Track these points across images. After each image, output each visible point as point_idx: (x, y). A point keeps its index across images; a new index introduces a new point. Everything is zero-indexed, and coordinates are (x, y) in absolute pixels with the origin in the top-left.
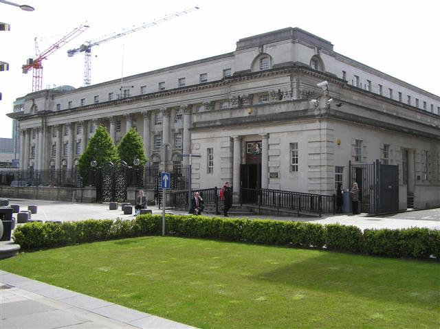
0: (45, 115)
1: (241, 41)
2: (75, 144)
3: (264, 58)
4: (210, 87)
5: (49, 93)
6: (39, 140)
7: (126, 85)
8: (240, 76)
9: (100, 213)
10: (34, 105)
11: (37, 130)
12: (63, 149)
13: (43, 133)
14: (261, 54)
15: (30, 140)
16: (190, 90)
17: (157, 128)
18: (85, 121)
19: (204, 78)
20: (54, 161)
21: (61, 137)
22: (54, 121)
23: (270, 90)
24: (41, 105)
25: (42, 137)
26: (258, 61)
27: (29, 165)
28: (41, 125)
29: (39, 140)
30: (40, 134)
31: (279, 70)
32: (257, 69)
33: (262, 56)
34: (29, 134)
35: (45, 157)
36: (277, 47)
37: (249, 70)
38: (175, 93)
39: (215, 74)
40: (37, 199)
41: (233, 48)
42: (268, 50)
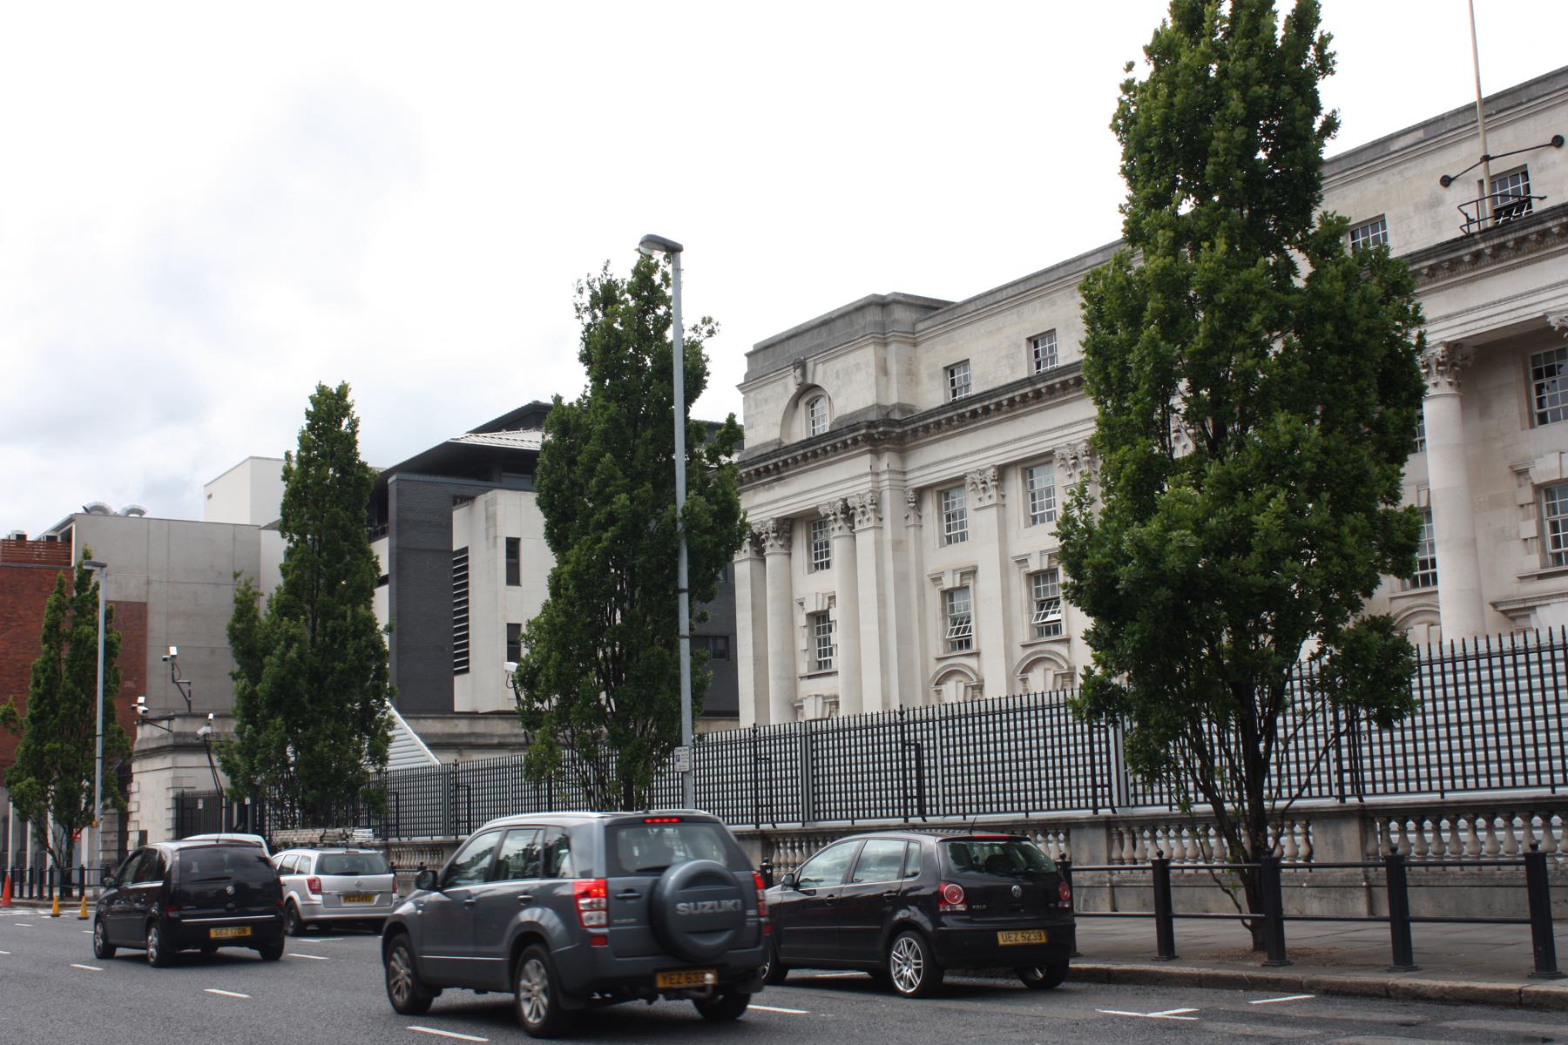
0: (890, 432)
24: (853, 386)
34: (788, 545)
38: (805, 457)
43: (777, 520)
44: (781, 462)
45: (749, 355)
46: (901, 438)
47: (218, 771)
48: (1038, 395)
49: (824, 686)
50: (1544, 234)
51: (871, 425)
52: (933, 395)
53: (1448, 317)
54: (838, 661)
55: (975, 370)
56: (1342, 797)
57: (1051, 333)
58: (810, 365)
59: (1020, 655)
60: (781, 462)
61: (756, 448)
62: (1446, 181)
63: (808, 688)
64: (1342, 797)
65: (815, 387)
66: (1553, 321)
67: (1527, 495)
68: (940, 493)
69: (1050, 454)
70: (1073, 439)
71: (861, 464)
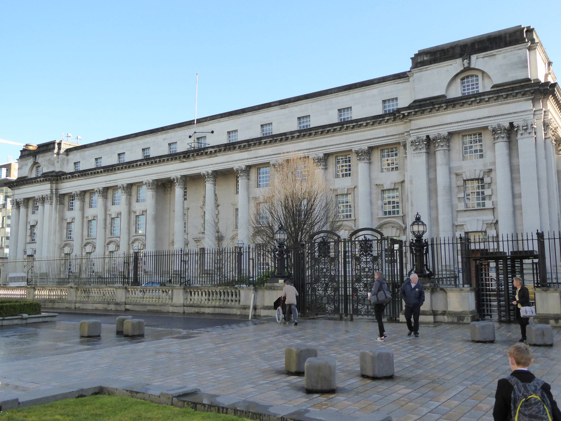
2: (109, 221)
3: (467, 77)
4: (101, 172)
6: (47, 215)
8: (433, 104)
9: (67, 345)
10: (35, 163)
11: (43, 200)
12: (108, 226)
13: (51, 204)
14: (468, 69)
16: (276, 140)
17: (90, 212)
18: (25, 199)
19: (147, 153)
20: (71, 247)
21: (82, 209)
26: (458, 81)
27: (25, 252)
28: (48, 192)
29: (47, 215)
30: (47, 206)
32: (456, 92)
33: (467, 73)
34: (27, 207)
36: (497, 56)
38: (140, 165)
39: (367, 105)
41: (406, 66)
42: (478, 61)
45: (412, 58)
47: (105, 306)
49: (33, 246)
52: (70, 168)
54: (37, 239)
55: (81, 164)
57: (236, 131)
62: (195, 132)
63: (29, 246)
65: (37, 163)
66: (235, 169)
68: (90, 193)
69: (269, 163)
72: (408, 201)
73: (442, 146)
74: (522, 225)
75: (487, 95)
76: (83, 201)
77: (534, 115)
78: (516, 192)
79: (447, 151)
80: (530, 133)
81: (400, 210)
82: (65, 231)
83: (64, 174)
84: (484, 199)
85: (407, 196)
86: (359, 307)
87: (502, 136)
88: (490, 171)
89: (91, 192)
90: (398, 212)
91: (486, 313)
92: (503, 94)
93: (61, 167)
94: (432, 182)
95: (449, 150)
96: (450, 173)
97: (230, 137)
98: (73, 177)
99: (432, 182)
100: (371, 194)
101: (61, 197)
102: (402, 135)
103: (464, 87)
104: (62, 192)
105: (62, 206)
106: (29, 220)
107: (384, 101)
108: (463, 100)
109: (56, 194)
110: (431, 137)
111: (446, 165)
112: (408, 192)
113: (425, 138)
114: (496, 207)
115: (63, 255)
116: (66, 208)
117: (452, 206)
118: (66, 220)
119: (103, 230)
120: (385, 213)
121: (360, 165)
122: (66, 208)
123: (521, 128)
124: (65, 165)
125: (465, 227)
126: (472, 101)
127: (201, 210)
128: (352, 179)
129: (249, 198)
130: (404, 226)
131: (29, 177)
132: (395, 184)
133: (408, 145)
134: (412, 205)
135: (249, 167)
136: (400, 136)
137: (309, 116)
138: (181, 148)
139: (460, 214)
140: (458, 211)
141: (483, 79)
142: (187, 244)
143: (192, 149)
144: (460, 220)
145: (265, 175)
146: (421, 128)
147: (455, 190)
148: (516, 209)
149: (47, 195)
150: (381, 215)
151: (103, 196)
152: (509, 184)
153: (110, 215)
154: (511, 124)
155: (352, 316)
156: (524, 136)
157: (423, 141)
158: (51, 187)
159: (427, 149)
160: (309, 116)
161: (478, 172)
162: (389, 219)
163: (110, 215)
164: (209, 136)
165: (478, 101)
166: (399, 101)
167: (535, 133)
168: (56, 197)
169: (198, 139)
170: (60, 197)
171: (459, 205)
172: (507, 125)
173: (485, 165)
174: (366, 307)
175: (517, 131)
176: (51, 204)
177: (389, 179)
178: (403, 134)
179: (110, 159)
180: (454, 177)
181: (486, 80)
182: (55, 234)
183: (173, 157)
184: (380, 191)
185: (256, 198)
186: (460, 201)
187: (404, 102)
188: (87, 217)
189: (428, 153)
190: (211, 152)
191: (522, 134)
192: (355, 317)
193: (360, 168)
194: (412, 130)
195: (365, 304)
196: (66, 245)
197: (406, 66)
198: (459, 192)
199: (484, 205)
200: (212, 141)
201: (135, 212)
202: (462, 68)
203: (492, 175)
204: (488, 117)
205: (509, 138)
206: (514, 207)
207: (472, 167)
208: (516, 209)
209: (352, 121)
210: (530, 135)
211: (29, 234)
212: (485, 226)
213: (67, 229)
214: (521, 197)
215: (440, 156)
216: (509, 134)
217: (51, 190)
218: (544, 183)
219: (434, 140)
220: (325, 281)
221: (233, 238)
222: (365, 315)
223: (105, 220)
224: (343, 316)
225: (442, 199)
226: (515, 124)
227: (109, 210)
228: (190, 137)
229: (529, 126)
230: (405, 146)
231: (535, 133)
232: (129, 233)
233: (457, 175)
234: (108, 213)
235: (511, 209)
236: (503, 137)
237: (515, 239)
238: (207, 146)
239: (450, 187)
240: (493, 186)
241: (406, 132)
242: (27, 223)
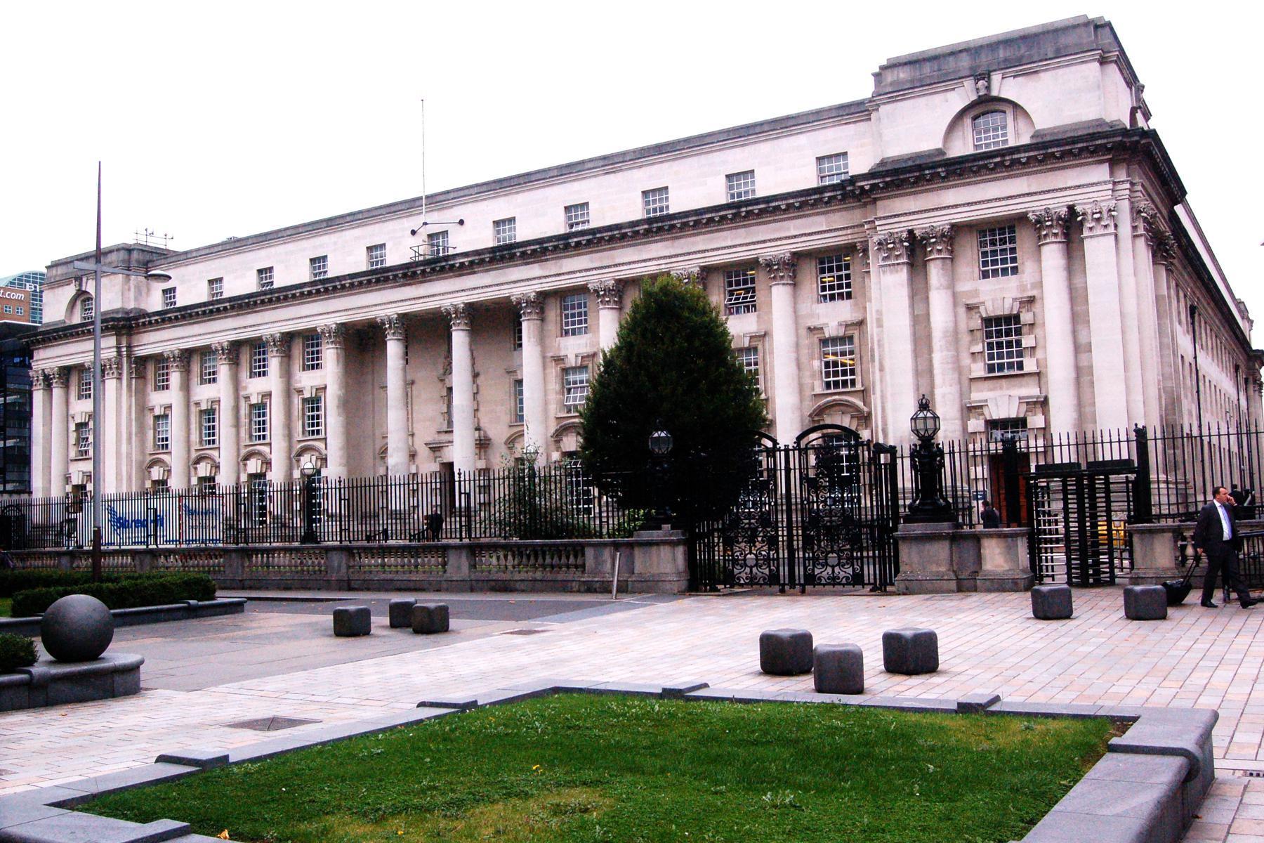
0: (126, 325)
1: (893, 65)
5: (135, 255)
7: (434, 217)
13: (119, 379)
15: (67, 403)
22: (152, 343)
23: (1033, 207)
24: (113, 295)
25: (119, 389)
26: (968, 121)
27: (67, 479)
31: (1056, 150)
32: (963, 146)
33: (986, 106)
34: (66, 385)
35: (129, 455)
37: (940, 152)
40: (1113, 717)
41: (865, 89)
43: (60, 368)
44: (63, 333)
46: (130, 328)
48: (270, 301)
50: (673, 227)
51: (118, 320)
53: (540, 278)
56: (461, 539)
58: (84, 279)
59: (194, 455)
60: (63, 333)
61: (48, 325)
62: (425, 224)
64: (461, 539)
66: (514, 299)
67: (977, 323)
70: (455, 301)
71: (1101, 173)
72: (873, 361)
73: (939, 251)
74: (1094, 404)
75: (1025, 151)
76: (187, 371)
77: (1113, 191)
78: (1083, 339)
79: (948, 262)
80: (1106, 226)
81: (858, 378)
82: (150, 433)
83: (145, 314)
84: (1020, 354)
85: (872, 350)
86: (817, 571)
87: (1055, 231)
88: (1031, 301)
89: (205, 352)
90: (853, 382)
91: (1044, 573)
92: (1055, 150)
93: (136, 299)
94: (920, 322)
95: (952, 260)
96: (955, 304)
97: (498, 232)
98: (163, 321)
99: (920, 322)
100: (797, 345)
101: (141, 364)
102: (861, 229)
103: (979, 133)
104: (141, 352)
105: (140, 381)
106: (71, 412)
107: (820, 159)
108: (979, 160)
109: (129, 356)
110: (917, 233)
111: (948, 288)
112: (872, 343)
113: (905, 235)
114: (1043, 370)
115: (148, 484)
116: (150, 386)
117: (959, 370)
118: (152, 410)
119: (234, 430)
120: (828, 385)
121: (774, 289)
122: (150, 386)
123: (1090, 217)
124: (144, 294)
125: (986, 411)
126: (996, 164)
127: (440, 385)
128: (758, 317)
129: (544, 357)
130: (866, 409)
131: (68, 323)
132: (847, 326)
133: (873, 249)
134: (882, 369)
135: (543, 296)
136: (856, 230)
137: (666, 188)
138: (396, 256)
139: (975, 386)
140: (972, 380)
141: (1015, 119)
142: (413, 456)
143: (421, 258)
144: (977, 396)
145: (576, 311)
146: (898, 216)
147: (965, 338)
148: (1083, 376)
149: (109, 360)
150: (819, 389)
151: (230, 360)
152: (1068, 327)
153: (247, 398)
154: (1071, 208)
155: (803, 586)
156: (1094, 233)
157: (901, 241)
158: (119, 342)
159: (909, 257)
160: (666, 188)
161: (1008, 303)
162: (836, 397)
163: (247, 398)
164: (454, 230)
165: (1007, 163)
166: (851, 159)
167: (1116, 226)
168: (129, 363)
169: (430, 236)
170: (136, 363)
171: (974, 366)
172: (1063, 211)
173: (1022, 287)
174: (748, 570)
175: (1081, 223)
176: (119, 379)
177: (833, 316)
178: (862, 226)
179: (241, 282)
180: (962, 311)
181: (1022, 123)
182: (129, 439)
183: (379, 276)
184: (816, 341)
185: (558, 360)
186: (974, 361)
187: (860, 164)
188: (197, 404)
189: (911, 265)
190: (462, 264)
191: (1091, 229)
192: (808, 588)
193: (778, 296)
194: (880, 218)
195: (827, 564)
196: (154, 463)
197: (865, 89)
198: (973, 342)
199: (1020, 366)
200: (462, 242)
201: (300, 391)
202: (974, 97)
203: (1037, 307)
204: (1028, 194)
205: (1066, 235)
206: (1078, 369)
207: (998, 295)
208: (1083, 376)
209: (757, 201)
210: (1106, 232)
211: (72, 440)
212: (1024, 407)
213: (155, 429)
214: (1090, 351)
215: (936, 273)
216: (1068, 228)
217: (119, 348)
218: (1132, 323)
219: (923, 239)
220: (750, 524)
221: (512, 441)
222: (828, 584)
223: (237, 409)
224: (787, 588)
225: (940, 357)
226: (1079, 209)
227: (245, 388)
228: (413, 233)
229: (1105, 215)
230: (865, 251)
231: (1116, 226)
232: (289, 436)
233: (970, 308)
234: (242, 393)
235: (1072, 375)
236: (1056, 235)
237: (1083, 442)
238: (451, 252)
239: (956, 331)
240: (1038, 331)
241: (869, 222)
242: (67, 416)
